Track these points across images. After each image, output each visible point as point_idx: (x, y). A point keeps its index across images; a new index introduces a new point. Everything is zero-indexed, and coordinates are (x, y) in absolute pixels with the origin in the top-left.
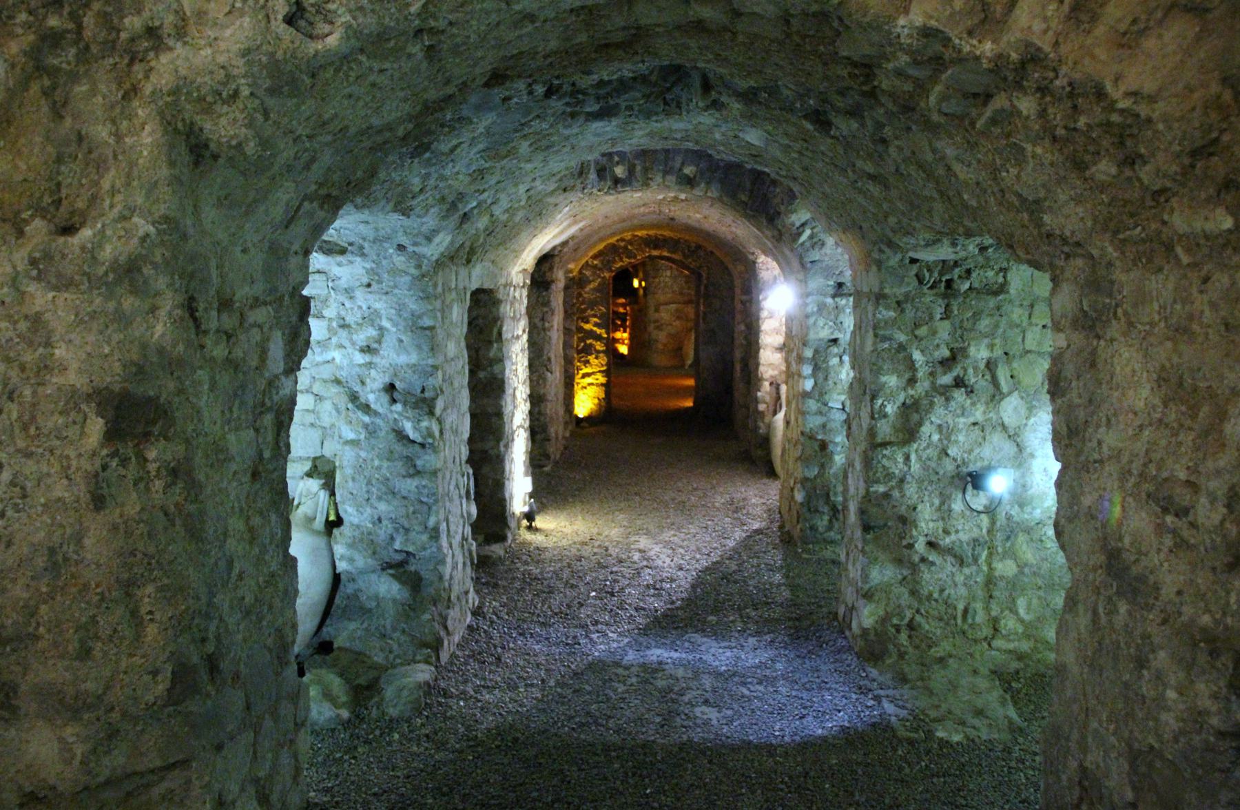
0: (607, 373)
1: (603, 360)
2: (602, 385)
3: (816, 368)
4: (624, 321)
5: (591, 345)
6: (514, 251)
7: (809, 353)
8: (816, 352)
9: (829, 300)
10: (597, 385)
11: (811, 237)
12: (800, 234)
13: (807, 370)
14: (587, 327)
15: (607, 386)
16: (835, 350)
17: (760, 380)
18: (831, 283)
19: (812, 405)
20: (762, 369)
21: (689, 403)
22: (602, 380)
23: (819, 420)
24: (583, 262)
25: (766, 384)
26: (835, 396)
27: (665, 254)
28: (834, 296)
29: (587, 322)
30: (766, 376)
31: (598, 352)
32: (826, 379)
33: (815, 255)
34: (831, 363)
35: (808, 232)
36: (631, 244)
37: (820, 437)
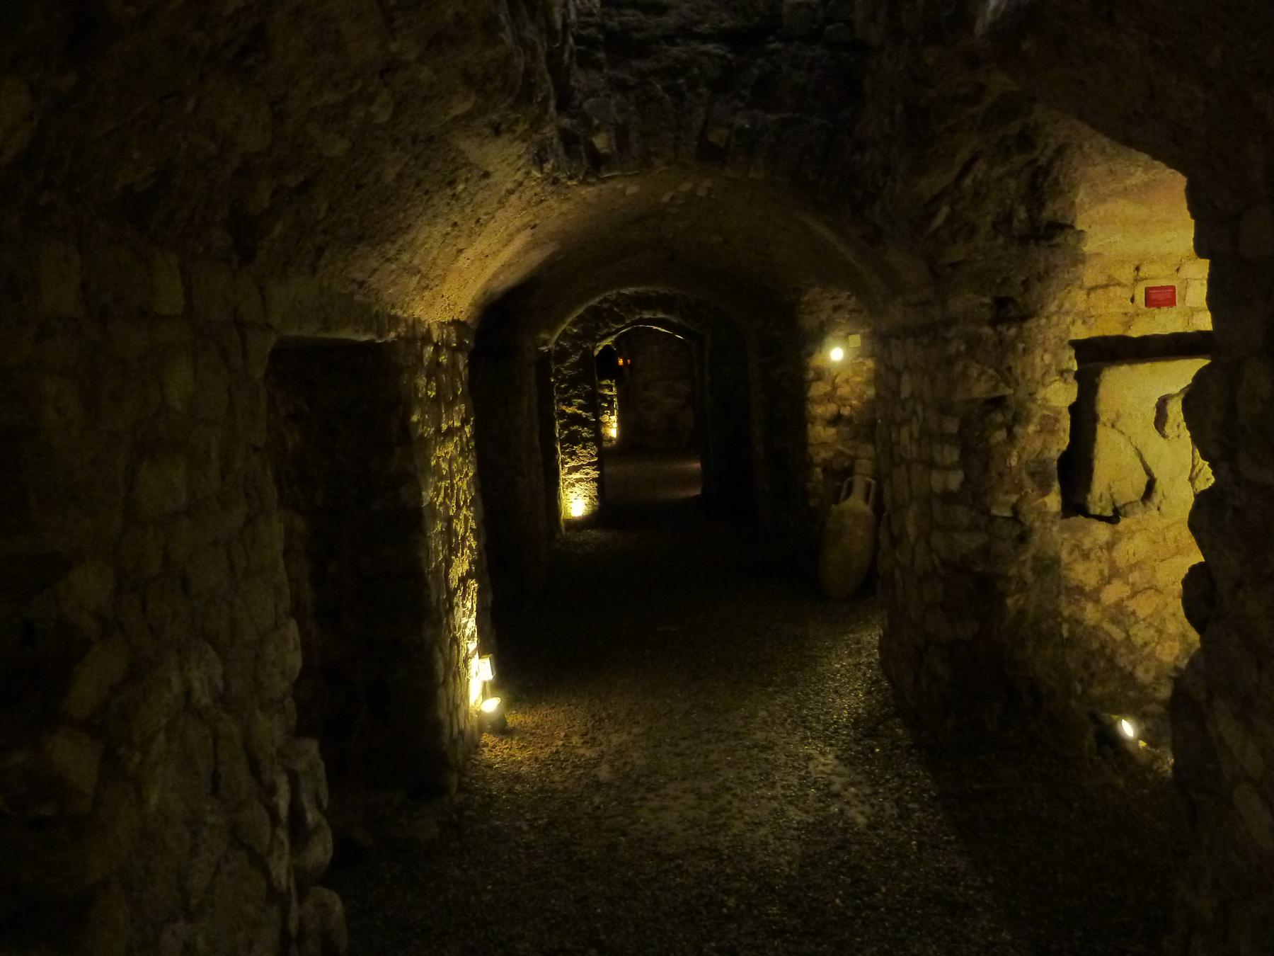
0: (599, 466)
1: (593, 450)
2: (594, 480)
3: (967, 452)
4: (611, 403)
5: (576, 431)
6: (413, 271)
7: (952, 426)
8: (965, 423)
9: (987, 331)
10: (587, 480)
11: (950, 219)
12: (932, 216)
13: (951, 454)
14: (569, 410)
15: (600, 482)
16: (999, 418)
17: (810, 465)
18: (987, 300)
19: (962, 515)
20: (811, 450)
21: (696, 492)
22: (595, 474)
23: (979, 539)
24: (560, 331)
25: (818, 470)
26: (1001, 497)
27: (660, 315)
28: (994, 323)
29: (570, 405)
30: (818, 459)
31: (586, 440)
32: (986, 468)
33: (958, 253)
34: (993, 441)
35: (945, 210)
36: (618, 305)
37: (979, 569)
